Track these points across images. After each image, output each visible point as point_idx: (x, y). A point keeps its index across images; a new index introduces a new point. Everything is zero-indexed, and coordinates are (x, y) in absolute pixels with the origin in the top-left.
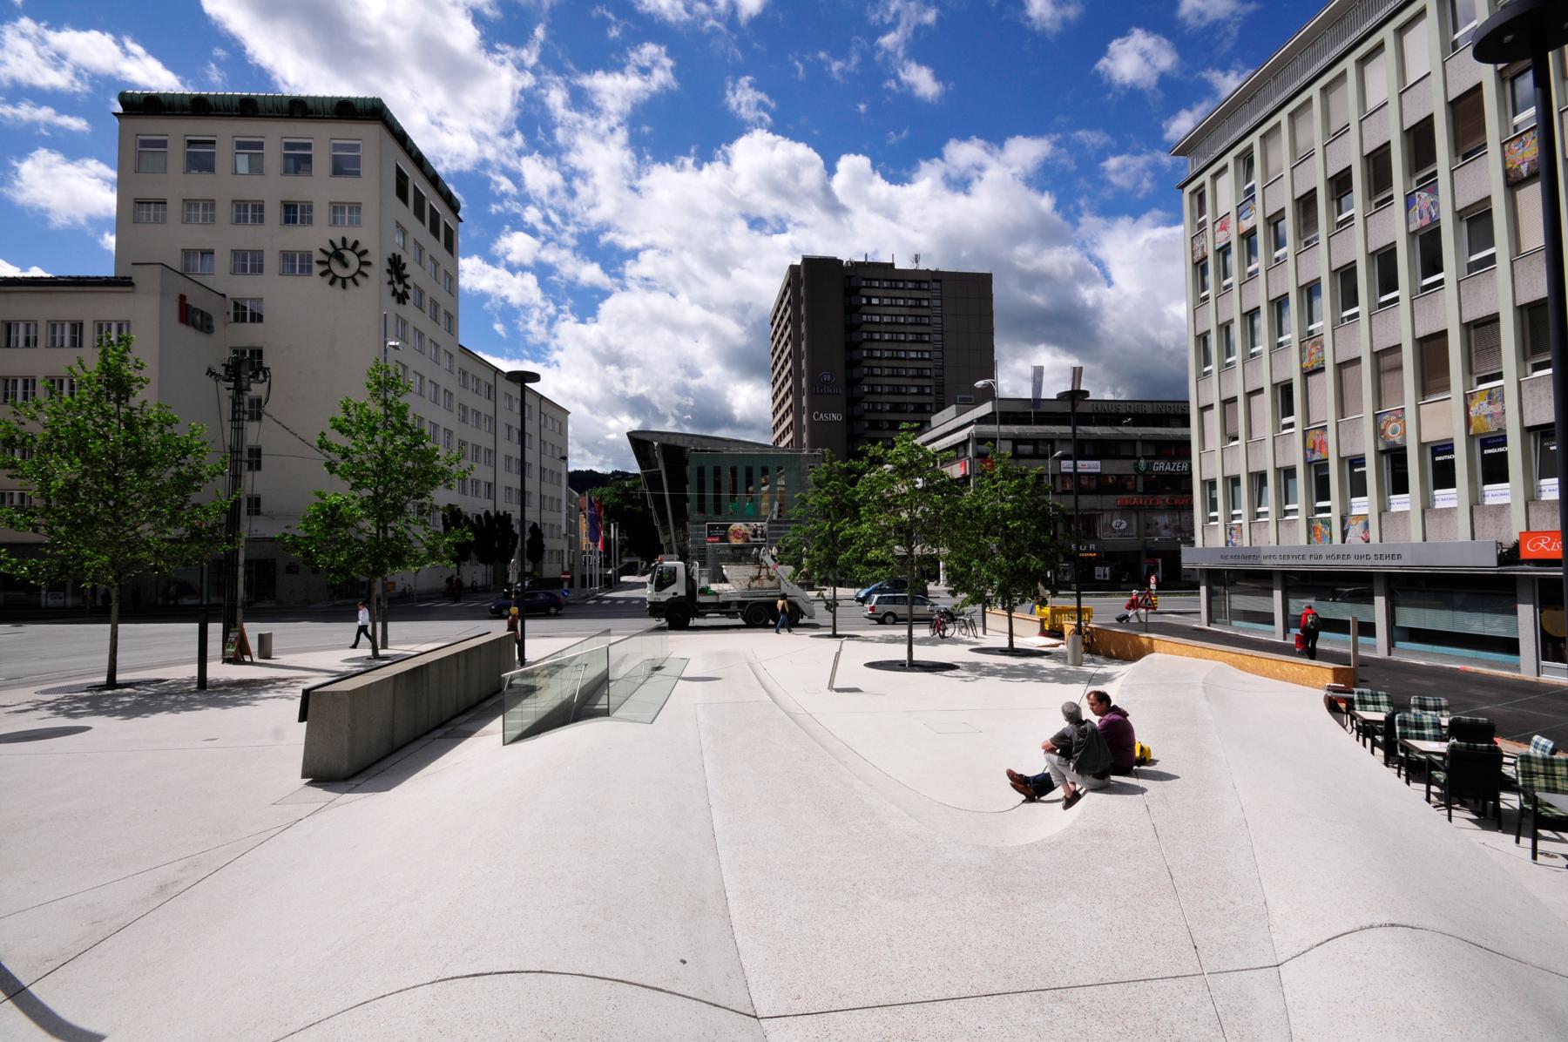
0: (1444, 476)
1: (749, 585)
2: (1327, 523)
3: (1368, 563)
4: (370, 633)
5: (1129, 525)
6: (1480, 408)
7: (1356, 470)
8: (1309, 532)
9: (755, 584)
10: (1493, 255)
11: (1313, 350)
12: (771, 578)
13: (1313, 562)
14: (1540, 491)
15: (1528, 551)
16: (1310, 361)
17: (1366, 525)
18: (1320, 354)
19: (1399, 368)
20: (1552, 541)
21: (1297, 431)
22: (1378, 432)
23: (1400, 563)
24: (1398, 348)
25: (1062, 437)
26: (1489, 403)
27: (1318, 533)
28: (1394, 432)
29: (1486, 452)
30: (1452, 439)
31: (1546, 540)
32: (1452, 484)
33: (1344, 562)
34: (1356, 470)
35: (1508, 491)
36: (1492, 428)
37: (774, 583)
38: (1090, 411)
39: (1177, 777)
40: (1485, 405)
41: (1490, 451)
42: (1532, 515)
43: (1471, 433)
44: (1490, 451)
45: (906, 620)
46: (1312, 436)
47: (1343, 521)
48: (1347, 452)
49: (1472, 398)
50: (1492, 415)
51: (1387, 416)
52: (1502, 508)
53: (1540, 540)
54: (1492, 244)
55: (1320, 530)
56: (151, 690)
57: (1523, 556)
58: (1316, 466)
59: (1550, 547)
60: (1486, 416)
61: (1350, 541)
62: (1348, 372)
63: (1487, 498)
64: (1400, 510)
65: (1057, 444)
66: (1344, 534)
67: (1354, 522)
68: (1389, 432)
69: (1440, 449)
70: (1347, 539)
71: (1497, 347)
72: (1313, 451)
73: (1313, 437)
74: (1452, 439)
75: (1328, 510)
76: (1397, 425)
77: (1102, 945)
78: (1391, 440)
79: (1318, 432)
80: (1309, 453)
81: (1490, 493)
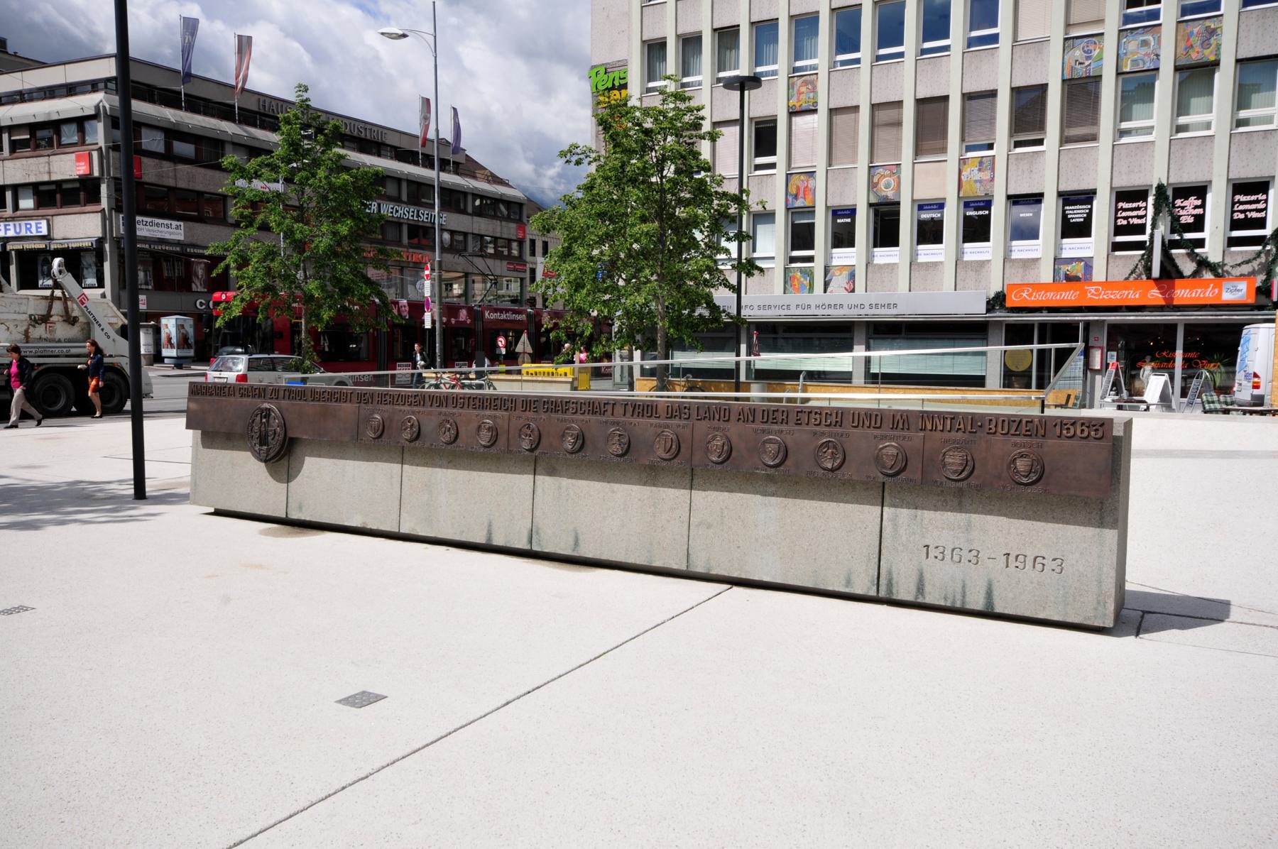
0: (930, 233)
1: (26, 333)
2: (809, 273)
3: (863, 312)
4: (1262, 277)
6: (971, 173)
7: (839, 221)
9: (39, 331)
10: (997, 34)
11: (803, 89)
12: (70, 320)
13: (820, 312)
14: (963, 253)
15: (1012, 301)
16: (799, 101)
17: (852, 276)
18: (811, 95)
19: (899, 124)
20: (1033, 291)
21: (780, 173)
22: (872, 185)
24: (899, 104)
25: (236, 140)
26: (980, 170)
27: (796, 282)
28: (887, 186)
29: (987, 212)
30: (945, 199)
31: (1028, 291)
32: (851, 243)
34: (839, 221)
35: (942, 251)
36: (980, 192)
37: (74, 331)
38: (255, 108)
40: (976, 171)
42: (1007, 271)
43: (961, 195)
46: (795, 181)
47: (827, 270)
48: (836, 202)
49: (965, 163)
50: (981, 181)
51: (881, 170)
52: (982, 264)
53: (1023, 291)
54: (995, 25)
57: (1008, 304)
58: (792, 213)
60: (976, 181)
61: (831, 292)
62: (839, 119)
63: (875, 258)
65: (228, 148)
66: (826, 285)
67: (837, 273)
68: (882, 185)
69: (839, 213)
70: (829, 290)
71: (992, 120)
72: (796, 197)
73: (798, 183)
74: (945, 199)
75: (810, 259)
76: (891, 180)
78: (883, 194)
79: (802, 177)
80: (790, 198)
81: (879, 254)
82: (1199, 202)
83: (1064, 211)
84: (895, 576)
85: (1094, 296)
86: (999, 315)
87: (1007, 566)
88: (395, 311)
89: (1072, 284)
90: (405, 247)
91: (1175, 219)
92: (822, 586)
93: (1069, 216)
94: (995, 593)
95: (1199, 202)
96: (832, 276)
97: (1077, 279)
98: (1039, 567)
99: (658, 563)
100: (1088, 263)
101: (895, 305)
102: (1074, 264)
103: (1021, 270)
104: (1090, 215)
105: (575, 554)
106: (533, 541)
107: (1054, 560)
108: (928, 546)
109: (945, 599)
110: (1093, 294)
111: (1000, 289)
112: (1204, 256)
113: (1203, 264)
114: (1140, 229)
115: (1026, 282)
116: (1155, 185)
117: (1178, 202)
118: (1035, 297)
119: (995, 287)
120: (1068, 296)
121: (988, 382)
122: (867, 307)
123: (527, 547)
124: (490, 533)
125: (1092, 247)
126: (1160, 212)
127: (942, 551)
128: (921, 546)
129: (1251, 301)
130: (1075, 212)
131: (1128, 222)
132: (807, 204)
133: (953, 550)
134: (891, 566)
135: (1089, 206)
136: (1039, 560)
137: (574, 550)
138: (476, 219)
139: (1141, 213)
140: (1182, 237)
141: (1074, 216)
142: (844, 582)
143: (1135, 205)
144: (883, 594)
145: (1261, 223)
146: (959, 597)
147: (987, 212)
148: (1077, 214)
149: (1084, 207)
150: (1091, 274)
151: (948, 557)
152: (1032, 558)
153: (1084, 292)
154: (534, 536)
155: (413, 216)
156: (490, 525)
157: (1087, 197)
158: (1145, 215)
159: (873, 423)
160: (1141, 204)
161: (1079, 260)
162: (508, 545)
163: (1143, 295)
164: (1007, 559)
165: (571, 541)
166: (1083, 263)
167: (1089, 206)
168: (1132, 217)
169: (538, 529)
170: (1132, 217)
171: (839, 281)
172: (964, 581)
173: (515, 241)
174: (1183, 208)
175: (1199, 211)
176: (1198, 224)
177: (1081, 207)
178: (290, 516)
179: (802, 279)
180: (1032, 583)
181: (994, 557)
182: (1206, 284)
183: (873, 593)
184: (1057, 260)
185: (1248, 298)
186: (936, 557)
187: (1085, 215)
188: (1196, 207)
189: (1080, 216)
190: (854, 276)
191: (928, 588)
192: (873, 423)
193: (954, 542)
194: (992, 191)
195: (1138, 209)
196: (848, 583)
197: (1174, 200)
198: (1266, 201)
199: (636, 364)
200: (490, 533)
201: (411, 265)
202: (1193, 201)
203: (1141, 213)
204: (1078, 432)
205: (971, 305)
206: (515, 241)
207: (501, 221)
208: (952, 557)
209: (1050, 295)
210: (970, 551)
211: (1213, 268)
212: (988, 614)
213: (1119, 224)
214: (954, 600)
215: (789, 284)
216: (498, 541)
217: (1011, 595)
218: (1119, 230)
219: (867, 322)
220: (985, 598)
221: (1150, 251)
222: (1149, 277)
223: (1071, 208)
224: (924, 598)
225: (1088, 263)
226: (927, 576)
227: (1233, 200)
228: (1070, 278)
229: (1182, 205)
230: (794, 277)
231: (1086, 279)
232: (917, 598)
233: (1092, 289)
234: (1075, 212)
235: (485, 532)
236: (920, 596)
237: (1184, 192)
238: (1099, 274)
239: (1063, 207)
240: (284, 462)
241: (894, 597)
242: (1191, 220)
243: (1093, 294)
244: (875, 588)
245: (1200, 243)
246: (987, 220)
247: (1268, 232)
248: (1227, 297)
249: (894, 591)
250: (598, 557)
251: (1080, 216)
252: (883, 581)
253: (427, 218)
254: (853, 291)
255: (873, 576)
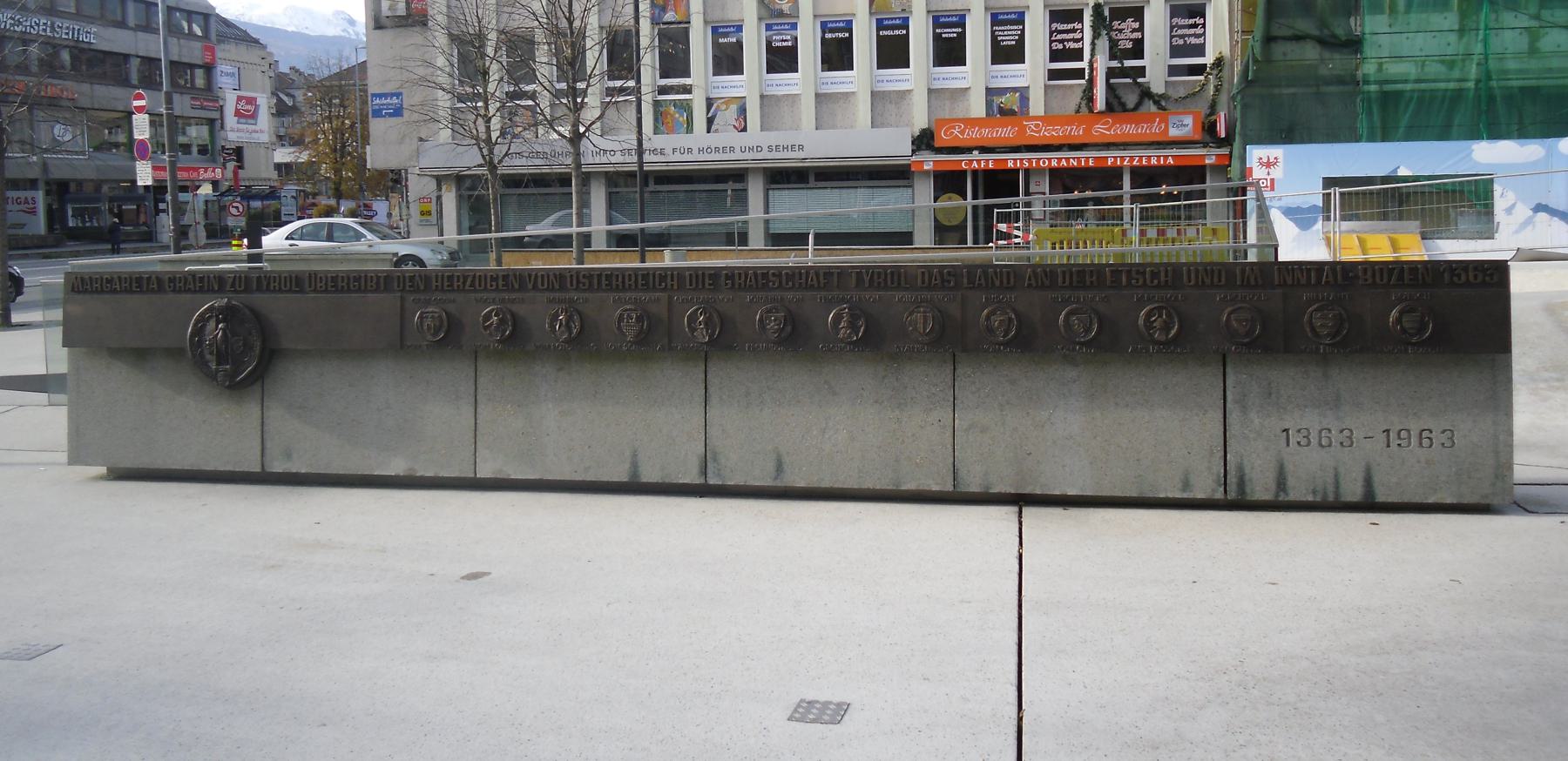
2: (686, 107)
5: (140, 109)
8: (656, 120)
13: (677, 157)
15: (943, 138)
17: (743, 111)
23: (801, 155)
27: (669, 120)
29: (904, 32)
33: (725, 157)
39: (490, 573)
41: (885, 33)
44: (885, 33)
45: (514, 181)
47: (710, 102)
55: (672, 116)
56: (723, 100)
59: (963, 135)
64: (841, 91)
66: (710, 121)
70: (713, 128)
77: (1304, 492)
78: (777, 7)
82: (1136, 25)
83: (993, 32)
84: (1247, 471)
85: (1036, 132)
86: (929, 161)
87: (1388, 446)
88: (1373, 88)
89: (1007, 119)
90: (34, 75)
91: (1113, 44)
92: (1149, 494)
93: (999, 38)
94: (1376, 480)
95: (1136, 25)
96: (716, 110)
97: (1011, 113)
98: (1426, 442)
99: (909, 485)
100: (1023, 93)
101: (801, 147)
102: (1008, 95)
103: (947, 102)
104: (1022, 36)
105: (779, 483)
106: (709, 471)
107: (1444, 432)
108: (1286, 430)
109: (1314, 492)
110: (1033, 131)
111: (925, 126)
112: (1146, 85)
113: (1146, 93)
114: (1077, 55)
115: (954, 116)
116: (1092, 4)
117: (1116, 23)
118: (968, 135)
119: (920, 122)
120: (1005, 133)
121: (916, 238)
122: (765, 149)
123: (698, 480)
124: (635, 465)
125: (1030, 73)
126: (1099, 35)
127: (1306, 434)
128: (1278, 431)
129: (1197, 137)
130: (1006, 33)
131: (1064, 46)
132: (678, 18)
133: (1320, 432)
134: (1242, 460)
135: (1021, 27)
136: (1425, 434)
137: (776, 478)
138: (141, 35)
139: (1077, 36)
140: (1123, 64)
141: (1004, 38)
142: (1180, 485)
143: (1070, 26)
144: (1232, 495)
145: (1200, 50)
146: (1331, 489)
147: (904, 32)
148: (1008, 37)
149: (1016, 27)
150: (1027, 107)
151: (1314, 441)
152: (1418, 432)
153: (1023, 129)
154: (708, 464)
155: (45, 30)
156: (634, 455)
157: (1076, 15)
158: (1082, 39)
159: (1216, 280)
160: (1077, 26)
161: (1015, 90)
162: (667, 481)
163: (1087, 131)
164: (1388, 436)
165: (771, 466)
166: (1018, 94)
167: (1021, 27)
168: (1068, 40)
169: (715, 454)
170: (1068, 40)
171: (728, 115)
172: (1336, 469)
173: (200, 67)
174: (1121, 31)
175: (1137, 35)
176: (1138, 50)
177: (1012, 28)
178: (268, 470)
179: (677, 115)
180: (1419, 462)
181: (1371, 435)
182: (1149, 119)
183: (1219, 495)
184: (990, 92)
185: (1194, 134)
186: (1299, 443)
187: (1017, 37)
188: (1134, 31)
189: (1012, 38)
190: (745, 110)
191: (1291, 482)
192: (1216, 280)
193: (1321, 422)
194: (910, 7)
195: (1074, 31)
196: (1186, 485)
197: (1111, 21)
198: (1204, 26)
199: (1126, 193)
200: (635, 465)
201: (45, 101)
202: (1131, 23)
203: (1199, 31)
204: (1471, 278)
205: (894, 144)
206: (200, 67)
207: (179, 39)
208: (1320, 440)
209: (985, 132)
210: (1342, 431)
211: (1158, 100)
212: (1369, 505)
213: (1054, 48)
214: (1325, 493)
215: (660, 122)
216: (649, 475)
217: (1394, 480)
218: (1055, 56)
219: (764, 168)
220: (1364, 486)
221: (1091, 82)
222: (1091, 111)
223: (1000, 28)
224: (1287, 495)
225: (1023, 93)
226: (1289, 467)
227: (1171, 23)
228: (1005, 112)
229: (1120, 27)
230: (668, 113)
231: (1022, 113)
232: (1277, 495)
233: (1032, 124)
234: (1006, 33)
235: (627, 466)
236: (1281, 493)
237: (1121, 14)
238: (1037, 106)
239: (992, 28)
240: (257, 387)
241: (1249, 498)
242: (1129, 45)
243: (1033, 131)
244: (1222, 489)
245: (1141, 71)
246: (848, 43)
247: (1209, 59)
248: (1174, 132)
249: (1248, 490)
250: (815, 486)
251: (1012, 38)
252: (1232, 479)
253: (67, 34)
254: (744, 129)
255: (1219, 476)
